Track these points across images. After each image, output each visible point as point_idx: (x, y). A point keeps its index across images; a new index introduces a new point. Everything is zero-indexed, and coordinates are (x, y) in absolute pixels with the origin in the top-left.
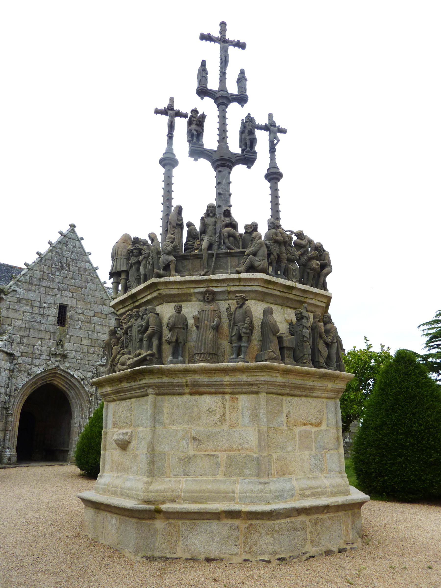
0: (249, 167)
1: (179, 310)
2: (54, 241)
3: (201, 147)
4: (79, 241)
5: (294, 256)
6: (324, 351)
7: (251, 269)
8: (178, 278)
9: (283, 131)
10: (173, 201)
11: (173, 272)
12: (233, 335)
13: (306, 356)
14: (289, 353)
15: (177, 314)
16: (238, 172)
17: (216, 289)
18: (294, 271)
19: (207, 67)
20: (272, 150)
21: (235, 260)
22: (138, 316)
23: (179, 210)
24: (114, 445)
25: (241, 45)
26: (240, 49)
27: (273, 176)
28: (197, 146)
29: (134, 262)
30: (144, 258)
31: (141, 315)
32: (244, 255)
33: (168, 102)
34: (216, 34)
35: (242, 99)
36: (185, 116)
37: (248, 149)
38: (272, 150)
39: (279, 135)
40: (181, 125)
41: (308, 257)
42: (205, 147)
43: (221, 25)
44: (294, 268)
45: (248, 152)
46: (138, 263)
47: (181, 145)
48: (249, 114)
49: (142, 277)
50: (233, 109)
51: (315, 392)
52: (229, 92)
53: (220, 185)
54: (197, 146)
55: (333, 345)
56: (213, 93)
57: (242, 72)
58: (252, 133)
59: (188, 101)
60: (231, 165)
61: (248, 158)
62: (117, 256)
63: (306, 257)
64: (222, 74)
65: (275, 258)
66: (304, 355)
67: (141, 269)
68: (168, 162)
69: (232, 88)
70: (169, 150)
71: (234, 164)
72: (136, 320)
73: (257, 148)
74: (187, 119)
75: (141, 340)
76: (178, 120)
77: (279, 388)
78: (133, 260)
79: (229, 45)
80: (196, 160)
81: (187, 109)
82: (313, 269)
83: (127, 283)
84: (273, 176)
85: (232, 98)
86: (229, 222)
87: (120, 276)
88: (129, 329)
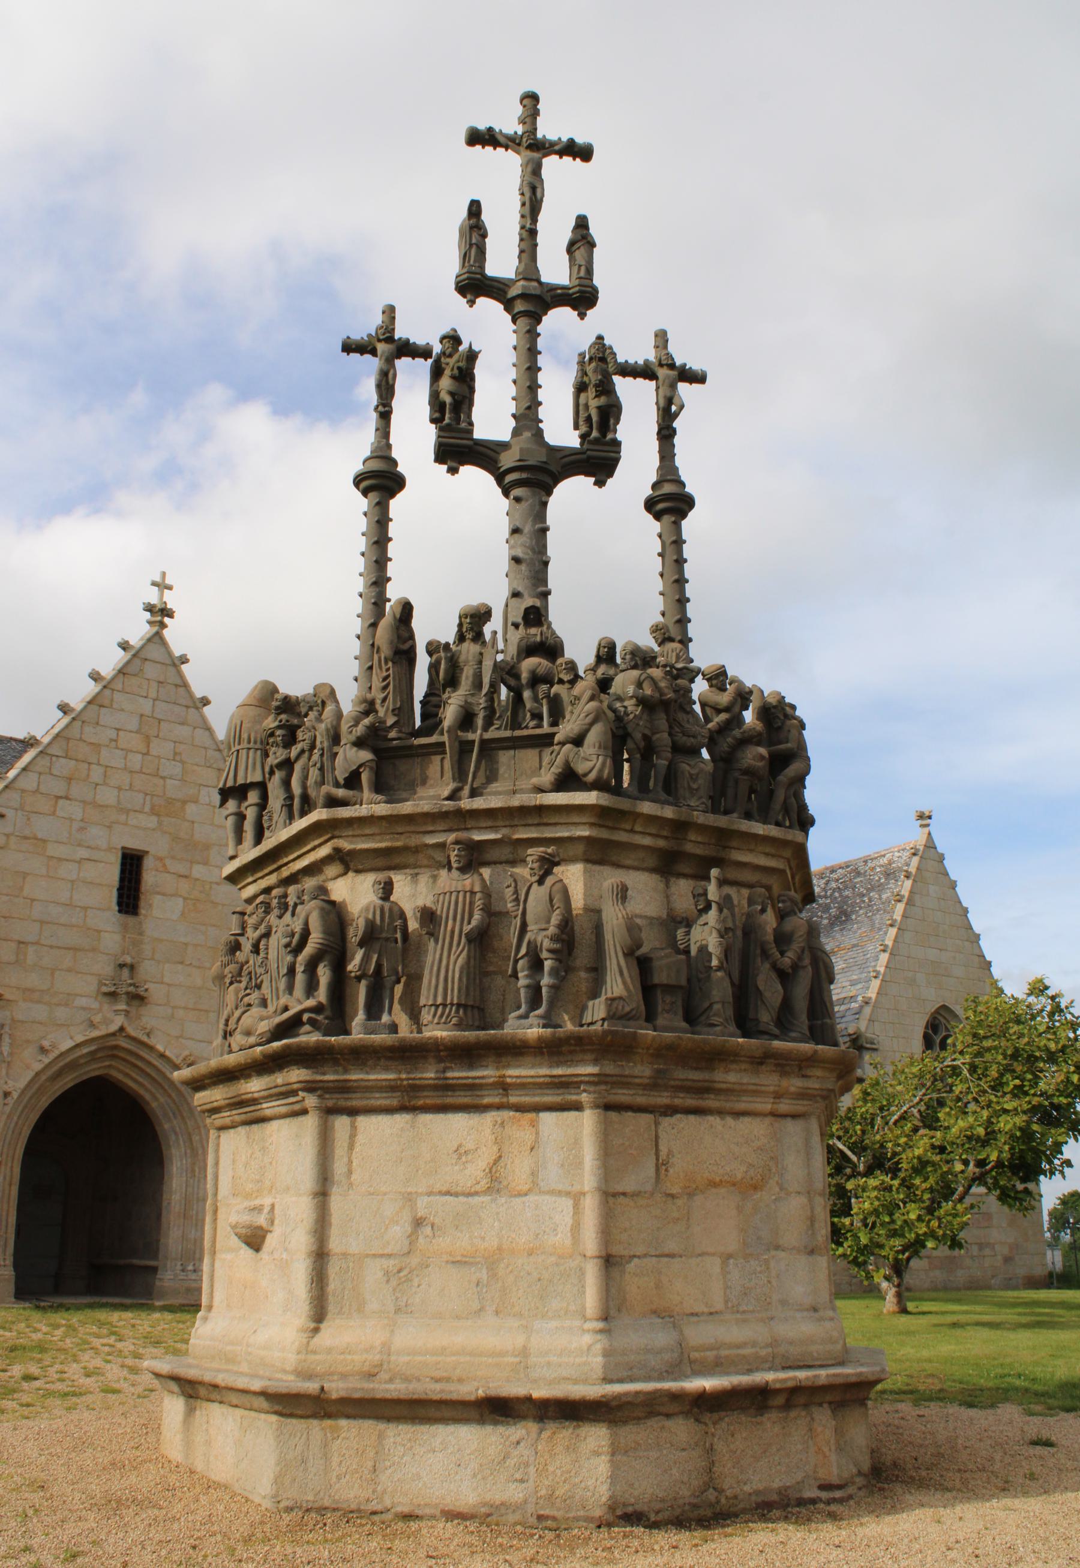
0: (600, 483)
2: (107, 670)
3: (467, 436)
4: (174, 665)
5: (694, 737)
6: (771, 990)
7: (568, 780)
8: (382, 809)
9: (697, 378)
10: (389, 585)
11: (367, 794)
12: (520, 955)
13: (716, 1007)
14: (668, 999)
15: (380, 902)
16: (572, 494)
17: (477, 837)
18: (693, 778)
19: (484, 217)
20: (666, 434)
22: (284, 907)
23: (407, 610)
24: (235, 1241)
25: (582, 152)
26: (578, 160)
27: (670, 503)
28: (453, 434)
30: (303, 751)
31: (291, 903)
32: (552, 744)
33: (378, 319)
34: (510, 124)
35: (582, 298)
36: (424, 353)
37: (595, 434)
38: (666, 434)
39: (683, 388)
40: (414, 387)
42: (477, 434)
43: (524, 102)
44: (693, 772)
45: (596, 441)
46: (287, 765)
47: (414, 437)
48: (600, 338)
49: (297, 802)
50: (559, 321)
51: (744, 1098)
52: (543, 279)
53: (516, 535)
54: (453, 434)
55: (801, 973)
56: (501, 286)
57: (582, 224)
58: (606, 389)
59: (431, 310)
60: (551, 482)
61: (598, 460)
62: (239, 744)
63: (729, 740)
64: (525, 234)
65: (638, 748)
66: (711, 1005)
68: (381, 481)
69: (554, 269)
70: (383, 452)
71: (557, 478)
72: (280, 917)
73: (623, 432)
74: (430, 361)
75: (291, 971)
76: (403, 364)
77: (641, 1092)
78: (277, 755)
79: (546, 155)
80: (453, 471)
81: (428, 335)
82: (748, 772)
83: (262, 816)
84: (670, 503)
85: (552, 297)
87: (245, 798)
88: (263, 942)
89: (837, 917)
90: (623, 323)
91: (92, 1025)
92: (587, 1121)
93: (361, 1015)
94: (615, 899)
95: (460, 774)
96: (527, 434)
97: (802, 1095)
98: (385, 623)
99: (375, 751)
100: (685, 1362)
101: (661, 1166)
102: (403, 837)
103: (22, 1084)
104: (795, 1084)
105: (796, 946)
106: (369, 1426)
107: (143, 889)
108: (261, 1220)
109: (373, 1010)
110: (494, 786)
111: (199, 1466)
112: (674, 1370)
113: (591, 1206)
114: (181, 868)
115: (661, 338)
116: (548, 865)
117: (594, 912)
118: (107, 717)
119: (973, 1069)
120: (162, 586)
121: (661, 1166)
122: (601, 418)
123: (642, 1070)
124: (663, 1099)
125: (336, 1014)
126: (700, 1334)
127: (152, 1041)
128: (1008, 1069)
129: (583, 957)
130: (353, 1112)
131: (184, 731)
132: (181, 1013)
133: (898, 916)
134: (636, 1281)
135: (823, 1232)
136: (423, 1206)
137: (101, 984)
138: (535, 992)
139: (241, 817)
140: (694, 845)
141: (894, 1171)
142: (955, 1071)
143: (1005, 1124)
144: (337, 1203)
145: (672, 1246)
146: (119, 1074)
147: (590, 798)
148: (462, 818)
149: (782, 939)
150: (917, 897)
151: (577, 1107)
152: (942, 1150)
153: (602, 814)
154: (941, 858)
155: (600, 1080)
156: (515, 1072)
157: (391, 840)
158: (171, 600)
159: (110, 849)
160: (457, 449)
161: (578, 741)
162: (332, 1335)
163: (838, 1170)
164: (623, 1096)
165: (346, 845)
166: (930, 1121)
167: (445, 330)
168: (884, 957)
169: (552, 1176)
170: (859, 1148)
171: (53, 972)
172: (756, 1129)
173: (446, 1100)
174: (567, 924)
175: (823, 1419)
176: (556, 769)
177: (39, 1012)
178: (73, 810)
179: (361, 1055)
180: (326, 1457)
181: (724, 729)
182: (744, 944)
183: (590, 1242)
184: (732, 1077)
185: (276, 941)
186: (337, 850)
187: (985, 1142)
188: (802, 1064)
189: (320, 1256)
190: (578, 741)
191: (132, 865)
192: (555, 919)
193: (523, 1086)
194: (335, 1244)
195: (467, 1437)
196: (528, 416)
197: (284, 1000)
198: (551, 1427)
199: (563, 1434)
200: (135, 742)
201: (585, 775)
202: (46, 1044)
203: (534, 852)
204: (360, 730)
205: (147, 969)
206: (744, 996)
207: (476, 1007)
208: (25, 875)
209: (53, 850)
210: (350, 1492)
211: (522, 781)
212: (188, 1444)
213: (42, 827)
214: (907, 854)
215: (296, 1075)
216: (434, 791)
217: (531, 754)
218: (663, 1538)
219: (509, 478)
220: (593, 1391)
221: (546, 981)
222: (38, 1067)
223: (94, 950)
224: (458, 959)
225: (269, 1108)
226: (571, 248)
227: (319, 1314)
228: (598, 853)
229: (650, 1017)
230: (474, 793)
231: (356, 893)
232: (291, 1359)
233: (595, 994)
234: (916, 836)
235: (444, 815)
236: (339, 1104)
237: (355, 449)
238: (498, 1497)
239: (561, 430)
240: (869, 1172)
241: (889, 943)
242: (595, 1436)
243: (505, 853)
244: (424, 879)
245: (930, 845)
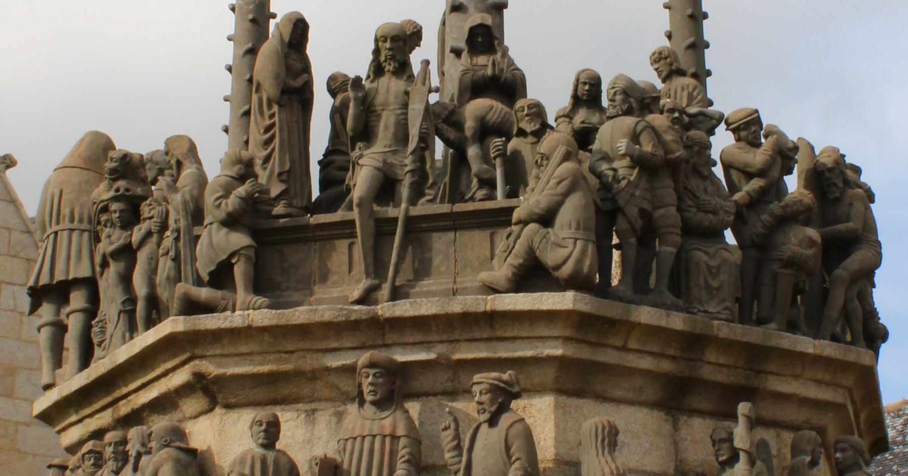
1: (271, 432)
7: (532, 274)
8: (263, 317)
11: (242, 295)
15: (261, 451)
17: (402, 356)
18: (713, 272)
21: (478, 239)
23: (299, 29)
29: (112, 248)
30: (149, 234)
32: (508, 223)
41: (772, 215)
44: (713, 263)
62: (58, 223)
65: (633, 229)
78: (112, 239)
82: (792, 263)
83: (91, 327)
86: (489, 72)
95: (377, 266)
102: (294, 357)
110: (426, 284)
116: (503, 397)
139: (60, 329)
140: (714, 369)
148: (380, 330)
153: (581, 325)
157: (277, 361)
161: (546, 219)
165: (211, 369)
176: (515, 260)
186: (199, 376)
190: (546, 219)
201: (557, 268)
203: (483, 379)
204: (232, 203)
211: (466, 276)
216: (338, 290)
228: (576, 381)
230: (396, 294)
243: (441, 380)
244: (324, 418)
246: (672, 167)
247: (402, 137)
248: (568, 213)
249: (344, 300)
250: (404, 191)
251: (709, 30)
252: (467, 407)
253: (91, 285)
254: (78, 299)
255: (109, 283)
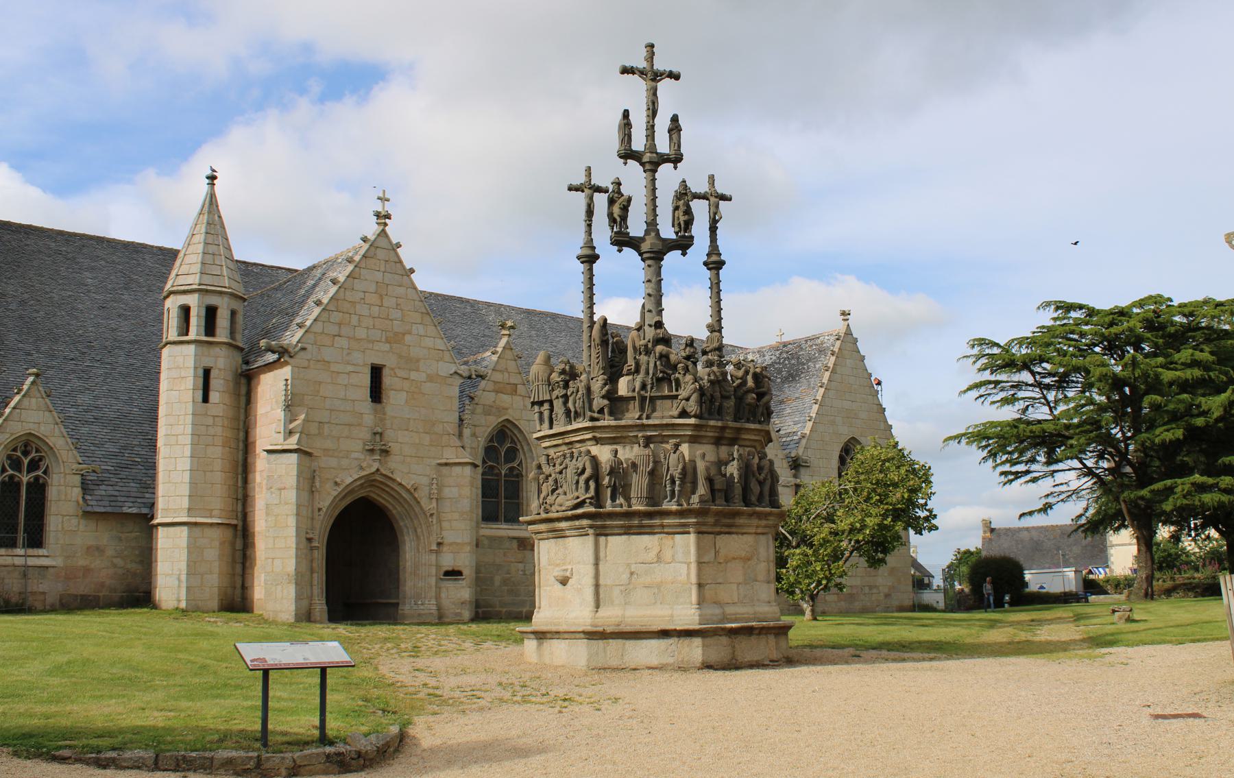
6: (755, 488)
7: (684, 414)
8: (613, 423)
20: (713, 229)
27: (715, 264)
35: (676, 159)
38: (713, 229)
47: (602, 234)
50: (665, 169)
57: (675, 119)
59: (609, 170)
67: (570, 405)
68: (590, 258)
69: (663, 146)
70: (590, 245)
75: (577, 482)
82: (749, 404)
84: (715, 264)
89: (787, 378)
90: (693, 173)
91: (362, 468)
92: (692, 538)
93: (609, 501)
94: (701, 456)
95: (642, 409)
96: (653, 234)
97: (766, 526)
98: (596, 327)
99: (609, 399)
100: (725, 619)
101: (717, 553)
103: (327, 503)
104: (763, 522)
105: (765, 472)
106: (620, 641)
107: (384, 387)
108: (568, 574)
109: (613, 499)
110: (655, 414)
111: (547, 661)
112: (721, 621)
113: (693, 567)
114: (401, 373)
115: (712, 179)
116: (677, 446)
117: (693, 462)
118: (358, 285)
119: (855, 490)
120: (383, 199)
121: (717, 553)
122: (685, 223)
123: (711, 520)
124: (718, 529)
125: (597, 500)
126: (730, 610)
127: (394, 476)
128: (874, 490)
129: (689, 478)
130: (606, 535)
131: (401, 291)
132: (408, 459)
133: (825, 381)
134: (708, 592)
135: (773, 575)
136: (633, 568)
137: (365, 444)
138: (673, 492)
139: (541, 413)
140: (728, 434)
141: (811, 545)
142: (846, 491)
143: (870, 521)
144: (601, 567)
145: (720, 580)
146: (376, 495)
147: (692, 421)
148: (643, 427)
149: (760, 468)
150: (838, 369)
151: (688, 533)
152: (836, 534)
153: (695, 426)
154: (856, 340)
155: (697, 523)
156: (666, 521)
158: (389, 208)
159: (365, 365)
160: (622, 240)
161: (688, 399)
162: (603, 612)
163: (781, 546)
164: (704, 529)
165: (598, 435)
166: (830, 519)
167: (612, 180)
168: (816, 407)
169: (680, 556)
170: (792, 533)
171: (339, 438)
172: (749, 539)
173: (641, 531)
174: (684, 468)
175: (772, 639)
176: (679, 409)
177: (333, 462)
178: (343, 342)
179: (611, 515)
180: (605, 652)
181: (740, 386)
182: (746, 470)
183: (694, 579)
184: (741, 521)
185: (570, 472)
187: (860, 531)
188: (765, 516)
189: (597, 586)
190: (688, 399)
191: (376, 372)
192: (680, 466)
193: (669, 526)
194: (601, 582)
195: (654, 643)
196: (652, 225)
197: (576, 494)
198: (682, 639)
199: (686, 641)
200: (373, 299)
202: (338, 480)
203: (672, 441)
204: (604, 392)
205: (389, 434)
206: (746, 490)
207: (653, 498)
208: (320, 383)
209: (334, 368)
210: (614, 663)
211: (666, 413)
212: (540, 655)
213: (327, 354)
214: (833, 338)
215: (585, 522)
216: (632, 416)
217: (669, 402)
218: (720, 673)
219: (645, 256)
220: (698, 627)
221: (677, 488)
222: (335, 493)
223: (359, 425)
224: (645, 481)
225: (568, 533)
226: (670, 131)
227: (597, 606)
228: (693, 440)
229: (713, 501)
230: (648, 417)
231: (604, 453)
232: (589, 621)
233: (694, 493)
234: (840, 327)
235: (636, 426)
236: (601, 532)
237: (577, 246)
238: (664, 662)
239: (667, 231)
240: (798, 546)
241: (819, 398)
242: (697, 642)
243: (659, 439)
244: (628, 448)
245: (848, 332)
246: (719, 382)
247: (647, 373)
248: (693, 398)
249: (633, 418)
250: (649, 387)
251: (723, 314)
252: (668, 446)
253: (551, 402)
254: (546, 406)
255: (558, 404)
